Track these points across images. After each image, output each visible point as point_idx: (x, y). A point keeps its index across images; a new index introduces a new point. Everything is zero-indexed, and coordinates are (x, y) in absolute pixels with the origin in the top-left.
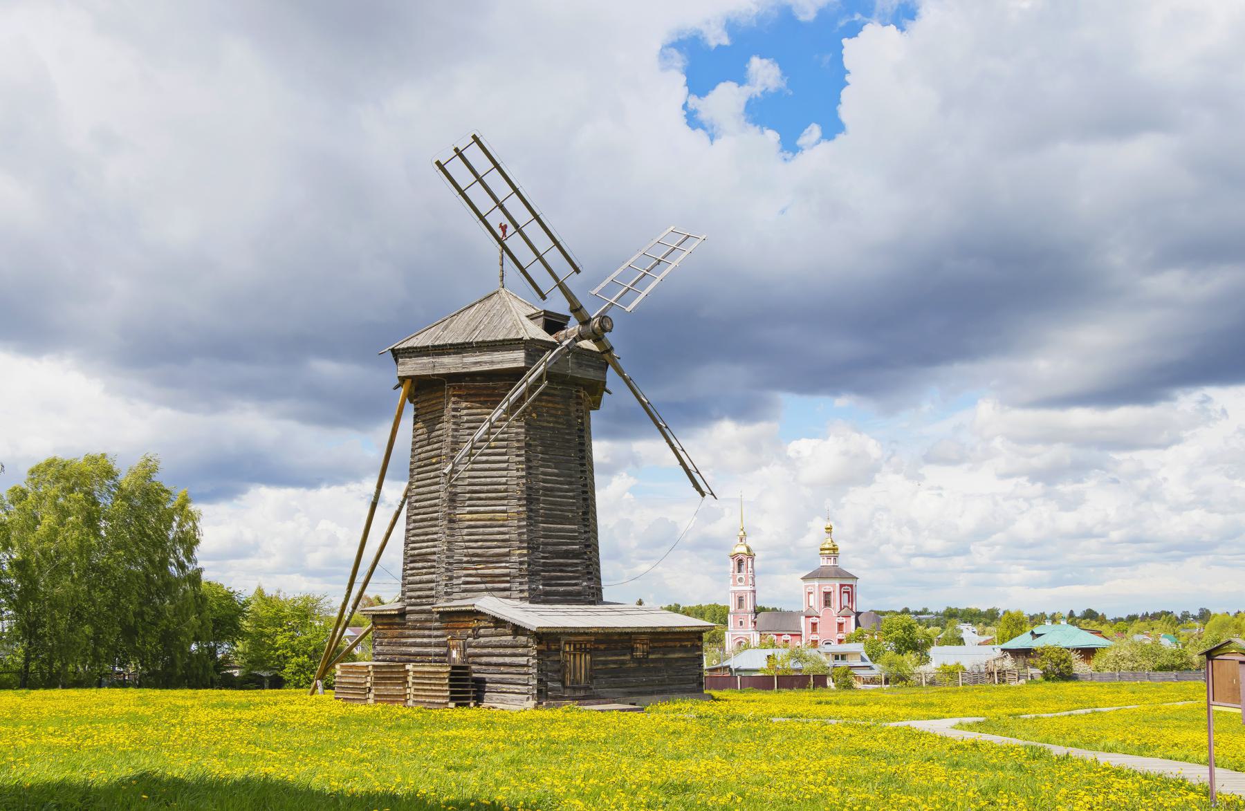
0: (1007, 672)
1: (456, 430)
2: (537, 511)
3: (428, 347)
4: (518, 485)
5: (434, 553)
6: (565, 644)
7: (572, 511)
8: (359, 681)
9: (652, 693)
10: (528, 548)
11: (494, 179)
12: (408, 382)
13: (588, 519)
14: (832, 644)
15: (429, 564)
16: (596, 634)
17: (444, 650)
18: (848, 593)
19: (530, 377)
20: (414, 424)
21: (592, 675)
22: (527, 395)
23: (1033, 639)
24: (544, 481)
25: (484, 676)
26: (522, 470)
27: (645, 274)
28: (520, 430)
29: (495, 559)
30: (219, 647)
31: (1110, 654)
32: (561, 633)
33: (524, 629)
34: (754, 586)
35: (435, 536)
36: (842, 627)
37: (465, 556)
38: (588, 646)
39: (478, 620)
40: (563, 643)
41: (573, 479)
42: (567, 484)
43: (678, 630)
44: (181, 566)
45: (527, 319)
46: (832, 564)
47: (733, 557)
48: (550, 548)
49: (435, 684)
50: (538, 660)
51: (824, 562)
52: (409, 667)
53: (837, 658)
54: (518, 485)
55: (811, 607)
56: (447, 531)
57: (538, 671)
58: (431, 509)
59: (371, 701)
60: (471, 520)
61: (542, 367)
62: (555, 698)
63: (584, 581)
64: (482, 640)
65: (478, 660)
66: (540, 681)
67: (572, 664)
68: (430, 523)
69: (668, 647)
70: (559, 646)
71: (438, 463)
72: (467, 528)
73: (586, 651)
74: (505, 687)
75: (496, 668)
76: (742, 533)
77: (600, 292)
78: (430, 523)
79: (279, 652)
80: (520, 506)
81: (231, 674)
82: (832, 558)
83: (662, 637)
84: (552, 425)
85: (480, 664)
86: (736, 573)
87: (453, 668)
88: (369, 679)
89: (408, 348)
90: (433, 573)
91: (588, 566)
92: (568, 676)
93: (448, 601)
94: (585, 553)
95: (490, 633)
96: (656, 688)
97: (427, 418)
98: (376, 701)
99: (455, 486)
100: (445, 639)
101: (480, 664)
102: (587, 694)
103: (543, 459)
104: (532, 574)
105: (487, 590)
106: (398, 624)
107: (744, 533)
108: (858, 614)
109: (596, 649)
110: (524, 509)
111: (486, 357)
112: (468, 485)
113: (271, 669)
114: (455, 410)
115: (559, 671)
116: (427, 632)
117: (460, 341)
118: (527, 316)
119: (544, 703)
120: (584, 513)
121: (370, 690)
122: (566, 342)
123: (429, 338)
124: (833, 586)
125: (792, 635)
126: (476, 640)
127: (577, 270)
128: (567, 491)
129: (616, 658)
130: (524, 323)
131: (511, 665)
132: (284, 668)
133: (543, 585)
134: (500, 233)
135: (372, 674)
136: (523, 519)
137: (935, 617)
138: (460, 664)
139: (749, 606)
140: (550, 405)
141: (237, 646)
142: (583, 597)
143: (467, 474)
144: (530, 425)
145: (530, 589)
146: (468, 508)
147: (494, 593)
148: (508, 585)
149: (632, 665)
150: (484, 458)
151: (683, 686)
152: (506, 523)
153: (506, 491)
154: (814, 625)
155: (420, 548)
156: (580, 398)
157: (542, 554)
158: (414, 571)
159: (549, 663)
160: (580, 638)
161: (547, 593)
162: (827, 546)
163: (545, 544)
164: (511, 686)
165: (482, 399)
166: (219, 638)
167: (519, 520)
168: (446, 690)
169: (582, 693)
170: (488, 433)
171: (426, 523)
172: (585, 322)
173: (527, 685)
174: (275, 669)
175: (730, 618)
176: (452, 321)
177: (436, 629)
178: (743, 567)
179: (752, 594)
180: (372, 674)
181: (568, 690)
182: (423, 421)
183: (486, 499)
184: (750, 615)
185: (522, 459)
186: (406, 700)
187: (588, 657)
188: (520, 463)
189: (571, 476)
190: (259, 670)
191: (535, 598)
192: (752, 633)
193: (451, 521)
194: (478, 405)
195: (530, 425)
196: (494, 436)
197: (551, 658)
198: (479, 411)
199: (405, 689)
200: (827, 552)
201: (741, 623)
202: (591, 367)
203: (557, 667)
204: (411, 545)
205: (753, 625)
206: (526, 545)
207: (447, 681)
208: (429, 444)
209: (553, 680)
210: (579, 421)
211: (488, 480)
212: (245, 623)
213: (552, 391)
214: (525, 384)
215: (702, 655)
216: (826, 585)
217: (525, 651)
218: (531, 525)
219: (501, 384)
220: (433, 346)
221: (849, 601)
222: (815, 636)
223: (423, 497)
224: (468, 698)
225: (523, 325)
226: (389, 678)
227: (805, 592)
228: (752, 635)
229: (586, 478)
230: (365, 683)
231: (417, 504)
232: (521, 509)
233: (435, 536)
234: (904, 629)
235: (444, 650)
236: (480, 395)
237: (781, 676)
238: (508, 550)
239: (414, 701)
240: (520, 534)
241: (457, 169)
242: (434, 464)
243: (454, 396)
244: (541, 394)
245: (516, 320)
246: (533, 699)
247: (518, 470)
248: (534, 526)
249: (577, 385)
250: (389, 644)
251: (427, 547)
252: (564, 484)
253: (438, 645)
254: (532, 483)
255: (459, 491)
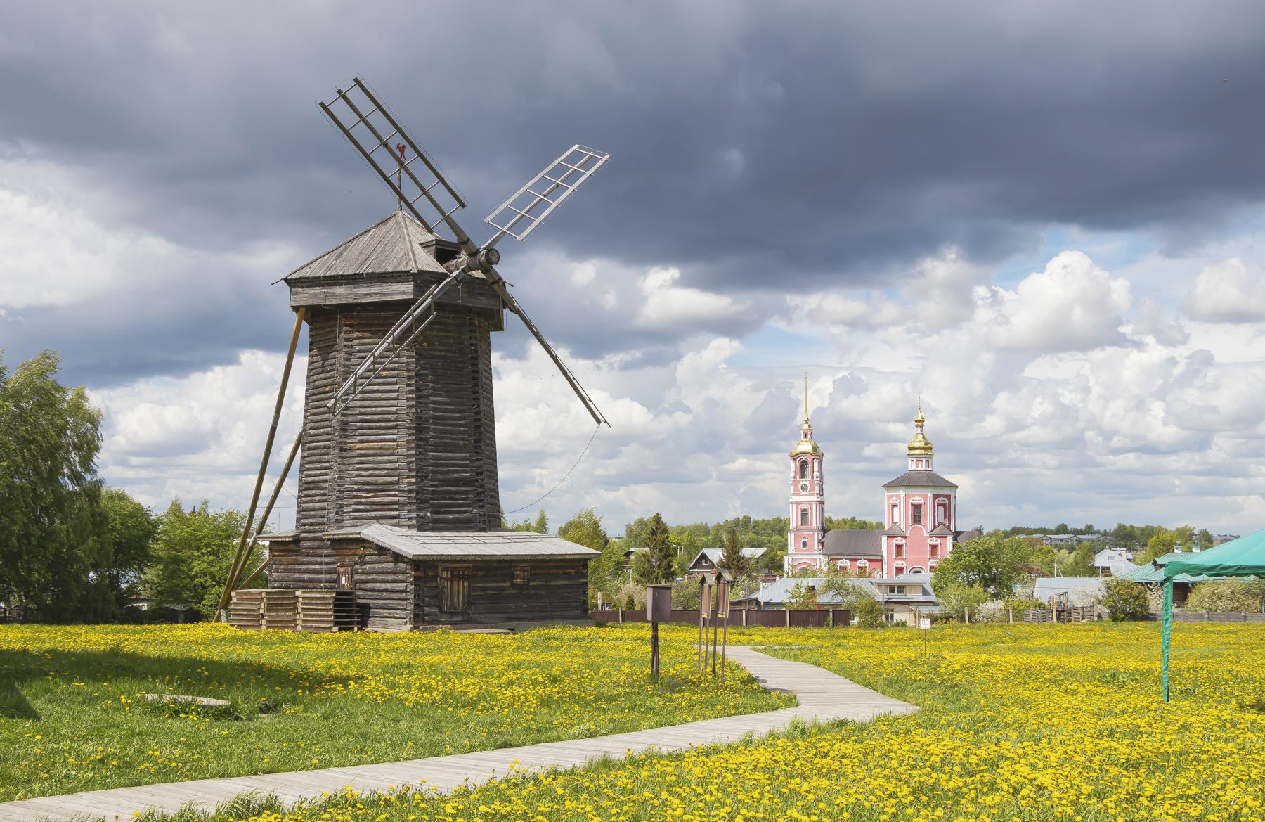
0: (1072, 611)
1: (348, 360)
2: (427, 440)
3: (319, 277)
4: (408, 414)
5: (326, 481)
6: (442, 570)
7: (463, 439)
8: (253, 608)
9: (533, 619)
10: (417, 476)
11: (377, 120)
12: (303, 309)
13: (480, 447)
14: (923, 572)
15: (322, 491)
16: (473, 561)
17: (334, 576)
18: (944, 505)
19: (415, 311)
20: (310, 351)
21: (470, 601)
22: (414, 328)
23: (1156, 570)
24: (435, 410)
25: (369, 601)
26: (412, 399)
27: (541, 199)
28: (410, 360)
29: (384, 487)
30: (123, 575)
31: (1205, 590)
32: (437, 560)
33: (403, 557)
34: (822, 495)
35: (327, 464)
36: (936, 550)
37: (356, 484)
38: (466, 573)
39: (364, 548)
40: (440, 569)
41: (465, 408)
42: (458, 413)
43: (560, 557)
44: (77, 478)
45: (419, 247)
46: (924, 468)
47: (794, 457)
48: (440, 476)
49: (321, 610)
50: (415, 585)
51: (913, 465)
52: (299, 593)
53: (892, 590)
54: (408, 414)
55: (895, 523)
56: (338, 460)
57: (415, 596)
58: (324, 437)
59: (263, 628)
60: (362, 449)
61: (429, 299)
62: (431, 622)
63: (475, 508)
64: (367, 567)
65: (364, 586)
66: (417, 606)
67: (449, 590)
68: (323, 451)
69: (549, 574)
70: (437, 573)
71: (331, 391)
72: (358, 456)
73: (464, 578)
74: (387, 612)
75: (379, 594)
76: (806, 427)
77: (492, 220)
78: (323, 451)
79: (197, 581)
80: (410, 435)
81: (137, 608)
82: (924, 460)
83: (544, 565)
84: (443, 354)
85: (365, 590)
86: (798, 479)
87: (338, 593)
88: (262, 605)
89: (300, 278)
90: (325, 501)
91: (479, 494)
92: (445, 601)
93: (338, 528)
94: (477, 481)
95: (374, 560)
96: (537, 614)
97: (321, 346)
98: (268, 627)
99: (347, 415)
100: (335, 566)
101: (365, 590)
102: (464, 618)
103: (433, 389)
104: (421, 502)
105: (375, 518)
106: (293, 551)
107: (809, 426)
108: (957, 535)
109: (474, 576)
110: (414, 438)
111: (375, 289)
112: (360, 414)
113: (186, 601)
114: (347, 339)
115: (436, 597)
116: (319, 559)
117: (351, 272)
118: (421, 244)
119: (421, 627)
120: (477, 441)
121: (263, 616)
122: (455, 274)
123: (321, 269)
124: (924, 497)
125: (870, 560)
126: (363, 567)
127: (463, 205)
128: (459, 419)
129: (495, 584)
130: (416, 252)
131: (392, 591)
132: (203, 599)
133: (431, 513)
134: (399, 154)
135: (265, 600)
136: (412, 448)
137: (1102, 538)
138: (346, 590)
139: (815, 522)
140: (442, 334)
141: (145, 574)
142: (473, 525)
143: (359, 403)
144: (420, 354)
145: (418, 517)
146: (359, 437)
147: (381, 521)
148: (397, 513)
149: (512, 592)
150: (375, 388)
151: (566, 613)
152: (396, 451)
153: (395, 420)
154: (899, 547)
155: (315, 476)
156: (475, 325)
157: (431, 483)
158: (308, 498)
159: (426, 589)
160: (458, 565)
161: (435, 521)
162: (917, 444)
163: (433, 472)
164: (392, 611)
165: (373, 329)
166: (124, 565)
167: (409, 449)
168: (331, 615)
169: (460, 618)
170: (355, 384)
171: (319, 451)
172: (473, 254)
173: (405, 610)
174: (190, 602)
175: (791, 538)
176: (345, 249)
177: (326, 556)
178: (808, 471)
179: (818, 506)
180: (265, 600)
181: (445, 615)
182: (318, 349)
183: (376, 428)
184: (816, 534)
185: (413, 388)
186: (296, 626)
187: (466, 584)
188: (410, 392)
189: (462, 404)
190: (171, 602)
191: (423, 526)
192: (817, 557)
193: (343, 450)
194: (369, 335)
195: (420, 354)
196: (361, 388)
197: (428, 585)
198: (370, 340)
199: (295, 615)
200: (917, 452)
201: (805, 544)
202: (482, 295)
203: (434, 592)
204: (306, 472)
205: (820, 547)
206: (414, 473)
207: (332, 606)
208: (323, 372)
209: (430, 605)
210: (473, 348)
211: (379, 409)
212: (156, 547)
213: (444, 320)
214: (411, 318)
215: (587, 583)
216: (915, 496)
217: (404, 577)
218: (420, 453)
219: (393, 313)
220: (325, 277)
221: (945, 517)
222: (900, 562)
223: (318, 424)
224: (352, 623)
225: (414, 255)
226: (281, 605)
227: (888, 504)
228: (818, 560)
229: (479, 406)
230: (259, 609)
231: (312, 432)
232: (410, 438)
233: (327, 464)
234: (978, 555)
235: (334, 576)
236: (371, 325)
237: (795, 611)
238: (397, 478)
239: (302, 627)
240: (409, 463)
241: (340, 109)
242: (327, 392)
243: (346, 325)
244: (431, 323)
245: (407, 250)
246: (410, 624)
247: (407, 399)
248: (423, 455)
249: (470, 312)
250: (285, 571)
251: (320, 475)
252: (455, 413)
253: (328, 572)
254: (421, 412)
255: (350, 420)
